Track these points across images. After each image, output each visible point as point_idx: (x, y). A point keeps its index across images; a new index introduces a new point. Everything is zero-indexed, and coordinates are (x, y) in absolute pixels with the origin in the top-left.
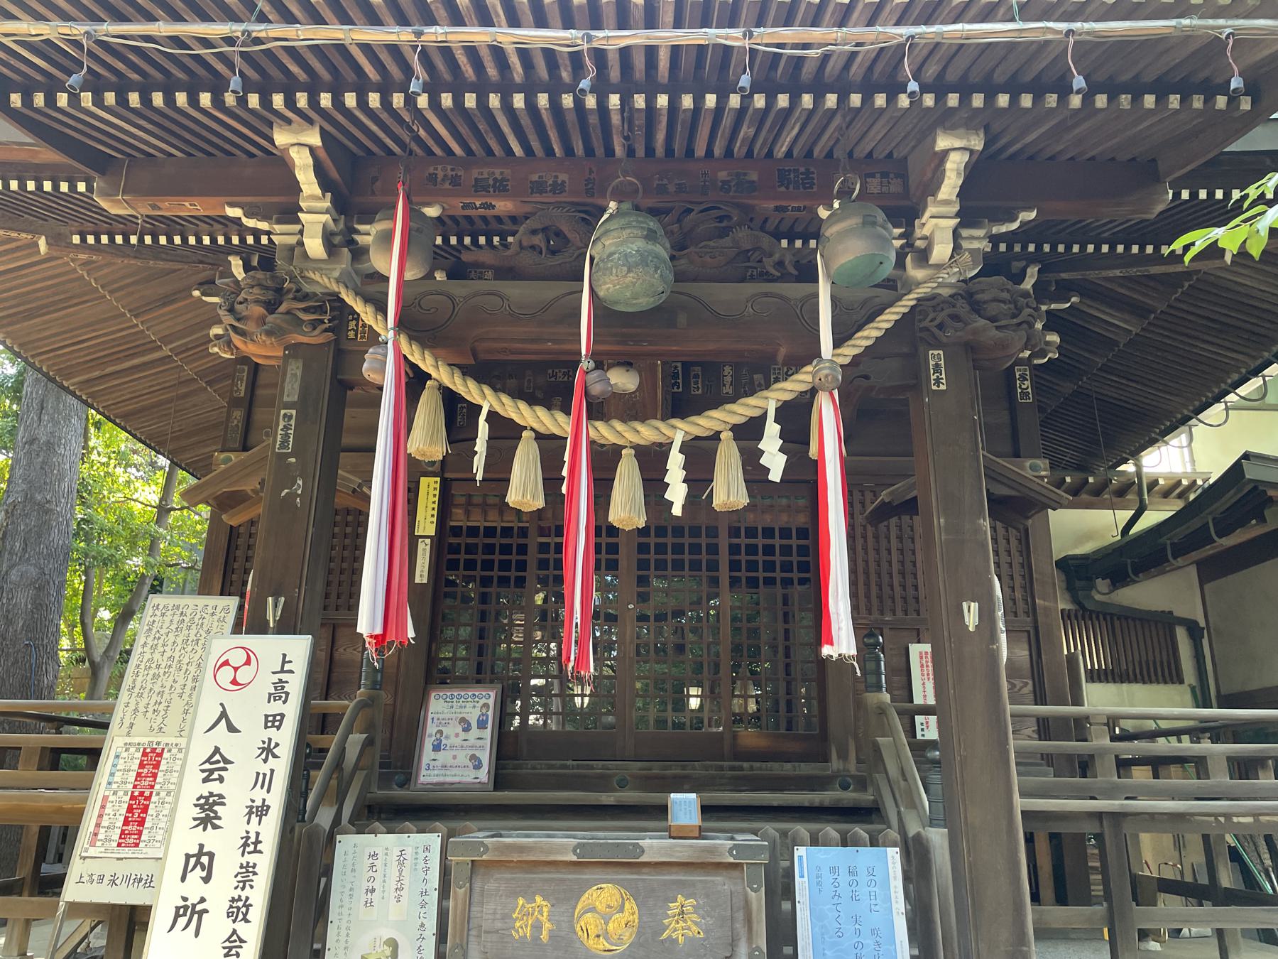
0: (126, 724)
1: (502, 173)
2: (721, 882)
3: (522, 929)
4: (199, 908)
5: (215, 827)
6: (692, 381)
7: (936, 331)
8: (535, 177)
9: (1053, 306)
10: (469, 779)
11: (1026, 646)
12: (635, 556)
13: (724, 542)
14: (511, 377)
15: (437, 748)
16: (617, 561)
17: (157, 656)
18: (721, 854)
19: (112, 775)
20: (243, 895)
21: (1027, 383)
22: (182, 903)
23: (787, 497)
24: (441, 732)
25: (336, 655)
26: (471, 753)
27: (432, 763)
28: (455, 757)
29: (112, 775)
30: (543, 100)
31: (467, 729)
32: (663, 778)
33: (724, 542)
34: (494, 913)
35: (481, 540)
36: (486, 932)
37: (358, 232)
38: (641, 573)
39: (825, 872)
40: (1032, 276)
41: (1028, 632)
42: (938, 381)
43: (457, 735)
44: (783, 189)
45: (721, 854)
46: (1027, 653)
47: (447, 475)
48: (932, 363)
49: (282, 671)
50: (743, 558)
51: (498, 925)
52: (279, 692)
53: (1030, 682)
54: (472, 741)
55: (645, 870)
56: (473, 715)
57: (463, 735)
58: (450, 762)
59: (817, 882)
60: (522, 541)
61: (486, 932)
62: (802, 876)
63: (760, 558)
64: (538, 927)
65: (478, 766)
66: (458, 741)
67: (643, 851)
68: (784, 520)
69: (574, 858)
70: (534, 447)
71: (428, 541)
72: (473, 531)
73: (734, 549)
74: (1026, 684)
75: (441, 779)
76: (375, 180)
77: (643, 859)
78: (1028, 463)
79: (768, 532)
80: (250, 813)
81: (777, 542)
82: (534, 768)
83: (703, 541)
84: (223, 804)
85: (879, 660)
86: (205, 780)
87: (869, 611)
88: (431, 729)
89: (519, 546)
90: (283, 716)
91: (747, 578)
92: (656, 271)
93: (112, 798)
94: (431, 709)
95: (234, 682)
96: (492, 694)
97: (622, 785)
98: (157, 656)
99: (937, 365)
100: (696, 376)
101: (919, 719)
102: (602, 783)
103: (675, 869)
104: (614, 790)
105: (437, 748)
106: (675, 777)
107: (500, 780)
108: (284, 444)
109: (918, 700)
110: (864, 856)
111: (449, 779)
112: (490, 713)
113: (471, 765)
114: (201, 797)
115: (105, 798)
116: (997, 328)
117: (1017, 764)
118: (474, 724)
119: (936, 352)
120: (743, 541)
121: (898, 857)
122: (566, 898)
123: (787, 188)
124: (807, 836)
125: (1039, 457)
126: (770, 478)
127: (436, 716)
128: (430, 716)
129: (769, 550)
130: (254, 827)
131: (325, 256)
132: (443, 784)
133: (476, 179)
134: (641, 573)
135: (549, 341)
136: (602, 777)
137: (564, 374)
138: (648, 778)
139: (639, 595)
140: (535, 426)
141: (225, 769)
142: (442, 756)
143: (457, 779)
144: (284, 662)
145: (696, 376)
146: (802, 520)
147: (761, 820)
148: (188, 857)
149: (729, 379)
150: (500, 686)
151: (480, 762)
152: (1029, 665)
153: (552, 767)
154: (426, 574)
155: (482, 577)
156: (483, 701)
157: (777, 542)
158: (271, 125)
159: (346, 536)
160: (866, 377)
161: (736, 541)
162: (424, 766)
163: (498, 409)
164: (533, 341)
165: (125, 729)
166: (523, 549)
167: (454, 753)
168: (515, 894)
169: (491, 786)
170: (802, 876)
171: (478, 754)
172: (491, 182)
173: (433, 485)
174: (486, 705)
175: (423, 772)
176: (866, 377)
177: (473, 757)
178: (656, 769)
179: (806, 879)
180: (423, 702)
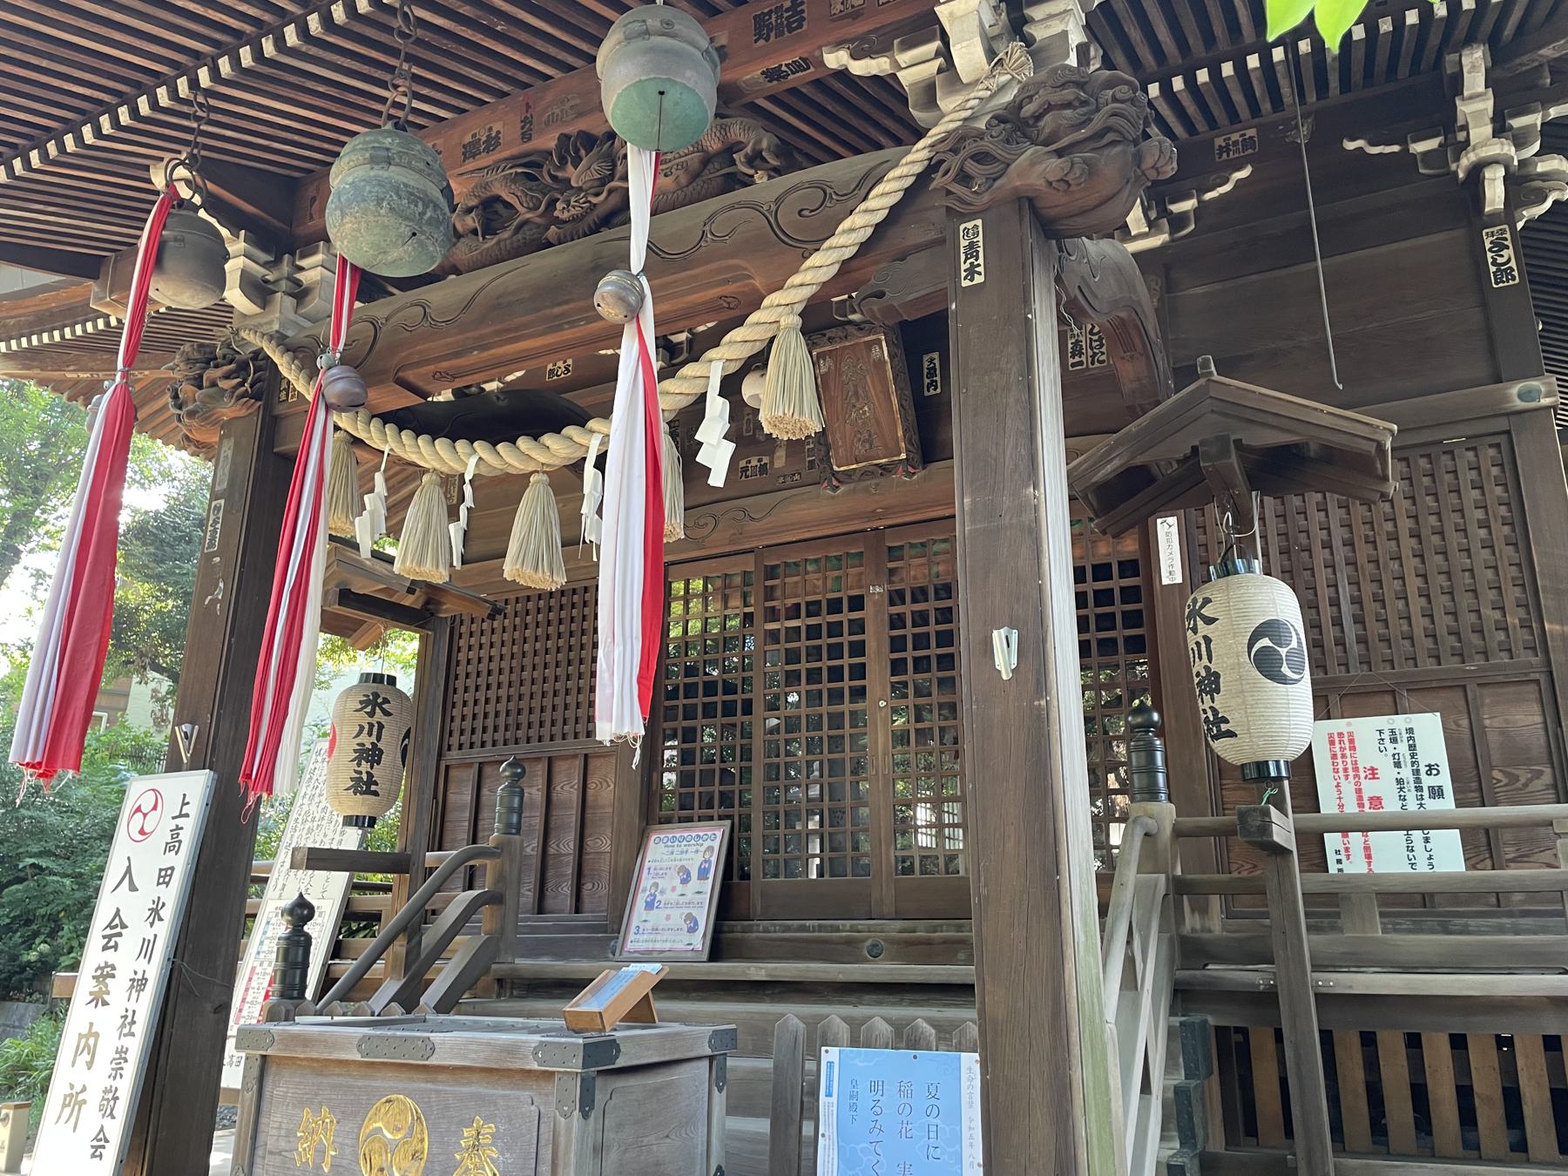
0: (280, 886)
2: (525, 1100)
3: (304, 1152)
4: (81, 1097)
5: (105, 1003)
7: (957, 189)
8: (468, 139)
9: (1554, 112)
10: (681, 946)
11: (1536, 708)
12: (888, 633)
15: (649, 906)
17: (313, 808)
18: (525, 1057)
19: (261, 943)
20: (115, 1084)
21: (1508, 253)
22: (69, 1091)
24: (656, 885)
25: (554, 796)
26: (687, 911)
27: (642, 925)
28: (668, 917)
29: (261, 943)
30: (1178, 83)
31: (685, 881)
32: (929, 942)
34: (279, 1128)
36: (271, 1153)
37: (301, 269)
38: (895, 656)
39: (863, 1089)
40: (1474, 68)
41: (1537, 682)
42: (971, 272)
43: (674, 889)
44: (762, 42)
45: (525, 1057)
46: (1539, 719)
48: (964, 243)
49: (181, 816)
51: (283, 1144)
52: (173, 846)
53: (1548, 771)
54: (690, 896)
55: (441, 1077)
56: (694, 862)
57: (680, 889)
58: (663, 923)
59: (851, 1102)
61: (271, 1153)
62: (829, 1095)
64: (321, 1152)
65: (692, 930)
66: (673, 897)
67: (433, 1049)
69: (358, 1057)
70: (437, 493)
74: (1539, 774)
75: (650, 946)
76: (313, 200)
77: (433, 1061)
78: (1515, 389)
80: (132, 987)
82: (766, 931)
84: (113, 976)
85: (1150, 751)
86: (105, 948)
88: (646, 882)
90: (172, 868)
92: (379, 204)
93: (259, 970)
94: (650, 855)
95: (142, 832)
96: (719, 834)
97: (875, 952)
98: (313, 808)
99: (972, 245)
101: (1332, 841)
102: (846, 950)
103: (475, 1077)
104: (865, 961)
105: (649, 906)
106: (946, 942)
107: (718, 949)
108: (211, 545)
109: (1328, 806)
110: (929, 1061)
111: (658, 946)
112: (714, 859)
113: (685, 928)
114: (99, 968)
115: (253, 969)
116: (1060, 153)
117: (1306, 914)
118: (694, 874)
119: (970, 225)
121: (977, 1068)
122: (353, 1112)
123: (767, 39)
124: (843, 1030)
125: (1538, 374)
126: (711, 482)
127: (653, 865)
128: (647, 865)
130: (131, 1006)
131: (258, 310)
132: (651, 952)
134: (895, 656)
135: (474, 349)
136: (849, 942)
138: (908, 943)
139: (893, 686)
140: (438, 466)
141: (120, 935)
142: (656, 916)
143: (667, 946)
144: (184, 804)
147: (913, 1003)
148: (81, 1036)
151: (696, 923)
152: (1543, 741)
153: (787, 929)
156: (706, 844)
158: (147, 168)
160: (881, 295)
162: (633, 929)
163: (399, 452)
164: (457, 355)
165: (278, 891)
167: (668, 912)
168: (301, 1104)
169: (705, 956)
170: (829, 1095)
171: (695, 913)
174: (710, 849)
175: (631, 937)
176: (881, 295)
177: (690, 917)
178: (922, 931)
179: (834, 1099)
180: (640, 846)
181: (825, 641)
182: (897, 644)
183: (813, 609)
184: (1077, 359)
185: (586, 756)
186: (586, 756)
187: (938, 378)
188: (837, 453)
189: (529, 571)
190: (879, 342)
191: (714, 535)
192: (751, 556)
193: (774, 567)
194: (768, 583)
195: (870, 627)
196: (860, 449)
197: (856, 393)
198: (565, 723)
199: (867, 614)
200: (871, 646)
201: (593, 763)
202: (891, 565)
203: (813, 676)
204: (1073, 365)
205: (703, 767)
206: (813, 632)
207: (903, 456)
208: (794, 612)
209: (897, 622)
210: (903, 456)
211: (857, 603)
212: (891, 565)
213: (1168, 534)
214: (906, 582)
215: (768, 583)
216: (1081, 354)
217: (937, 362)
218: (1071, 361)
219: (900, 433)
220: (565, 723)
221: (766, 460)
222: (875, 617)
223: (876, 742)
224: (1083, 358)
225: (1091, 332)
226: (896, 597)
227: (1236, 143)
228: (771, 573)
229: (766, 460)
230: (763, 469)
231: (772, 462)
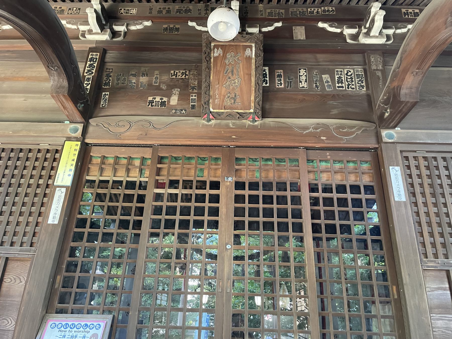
1: (302, 10)
6: (277, 79)
12: (233, 205)
13: (305, 195)
14: (143, 75)
16: (217, 209)
23: (353, 162)
33: (305, 195)
35: (121, 191)
47: (87, 141)
50: (321, 208)
60: (141, 192)
63: (336, 208)
68: (352, 180)
71: (64, 190)
72: (118, 183)
73: (315, 202)
79: (341, 189)
81: (349, 196)
83: (289, 194)
87: (436, 256)
89: (139, 196)
91: (326, 225)
96: (102, 325)
100: (280, 76)
120: (320, 195)
129: (343, 202)
133: (291, 12)
137: (183, 74)
145: (280, 76)
146: (114, 184)
149: (304, 78)
150: (111, 317)
154: (58, 216)
155: (121, 221)
157: (349, 196)
159: (38, 186)
161: (315, 195)
166: (141, 199)
172: (298, 13)
173: (74, 147)
181: (193, 204)
182: (238, 212)
183: (187, 184)
184: (340, 85)
185: (7, 259)
186: (7, 259)
187: (268, 79)
188: (214, 101)
189: (171, 7)
190: (251, 47)
191: (128, 133)
192: (149, 150)
193: (162, 158)
194: (159, 166)
195: (222, 199)
196: (228, 102)
197: (232, 71)
198: (24, 235)
199: (221, 192)
200: (222, 211)
201: (10, 265)
202: (237, 167)
203: (345, 216)
204: (338, 87)
205: (80, 275)
206: (187, 198)
207: (252, 111)
208: (173, 184)
209: (239, 199)
210: (252, 111)
211: (215, 185)
212: (237, 167)
213: (396, 175)
214: (246, 177)
215: (159, 166)
216: (342, 83)
217: (267, 71)
218: (337, 85)
219: (253, 98)
220: (24, 235)
221: (165, 99)
222: (226, 193)
223: (223, 270)
224: (343, 85)
225: (347, 74)
226: (239, 185)
227: (411, 13)
228: (161, 160)
229: (165, 99)
230: (163, 104)
231: (169, 101)
